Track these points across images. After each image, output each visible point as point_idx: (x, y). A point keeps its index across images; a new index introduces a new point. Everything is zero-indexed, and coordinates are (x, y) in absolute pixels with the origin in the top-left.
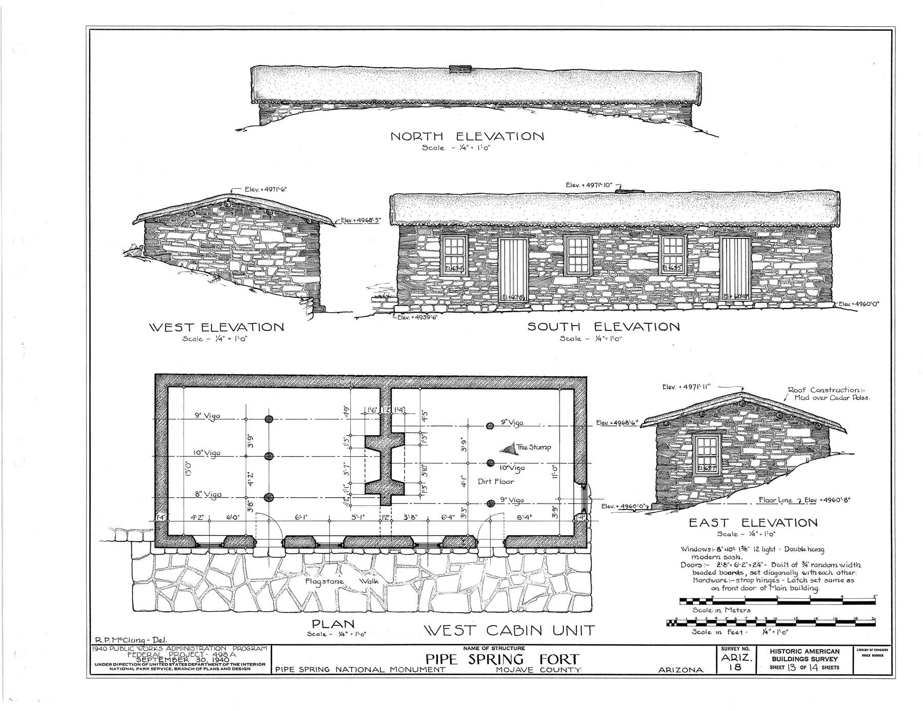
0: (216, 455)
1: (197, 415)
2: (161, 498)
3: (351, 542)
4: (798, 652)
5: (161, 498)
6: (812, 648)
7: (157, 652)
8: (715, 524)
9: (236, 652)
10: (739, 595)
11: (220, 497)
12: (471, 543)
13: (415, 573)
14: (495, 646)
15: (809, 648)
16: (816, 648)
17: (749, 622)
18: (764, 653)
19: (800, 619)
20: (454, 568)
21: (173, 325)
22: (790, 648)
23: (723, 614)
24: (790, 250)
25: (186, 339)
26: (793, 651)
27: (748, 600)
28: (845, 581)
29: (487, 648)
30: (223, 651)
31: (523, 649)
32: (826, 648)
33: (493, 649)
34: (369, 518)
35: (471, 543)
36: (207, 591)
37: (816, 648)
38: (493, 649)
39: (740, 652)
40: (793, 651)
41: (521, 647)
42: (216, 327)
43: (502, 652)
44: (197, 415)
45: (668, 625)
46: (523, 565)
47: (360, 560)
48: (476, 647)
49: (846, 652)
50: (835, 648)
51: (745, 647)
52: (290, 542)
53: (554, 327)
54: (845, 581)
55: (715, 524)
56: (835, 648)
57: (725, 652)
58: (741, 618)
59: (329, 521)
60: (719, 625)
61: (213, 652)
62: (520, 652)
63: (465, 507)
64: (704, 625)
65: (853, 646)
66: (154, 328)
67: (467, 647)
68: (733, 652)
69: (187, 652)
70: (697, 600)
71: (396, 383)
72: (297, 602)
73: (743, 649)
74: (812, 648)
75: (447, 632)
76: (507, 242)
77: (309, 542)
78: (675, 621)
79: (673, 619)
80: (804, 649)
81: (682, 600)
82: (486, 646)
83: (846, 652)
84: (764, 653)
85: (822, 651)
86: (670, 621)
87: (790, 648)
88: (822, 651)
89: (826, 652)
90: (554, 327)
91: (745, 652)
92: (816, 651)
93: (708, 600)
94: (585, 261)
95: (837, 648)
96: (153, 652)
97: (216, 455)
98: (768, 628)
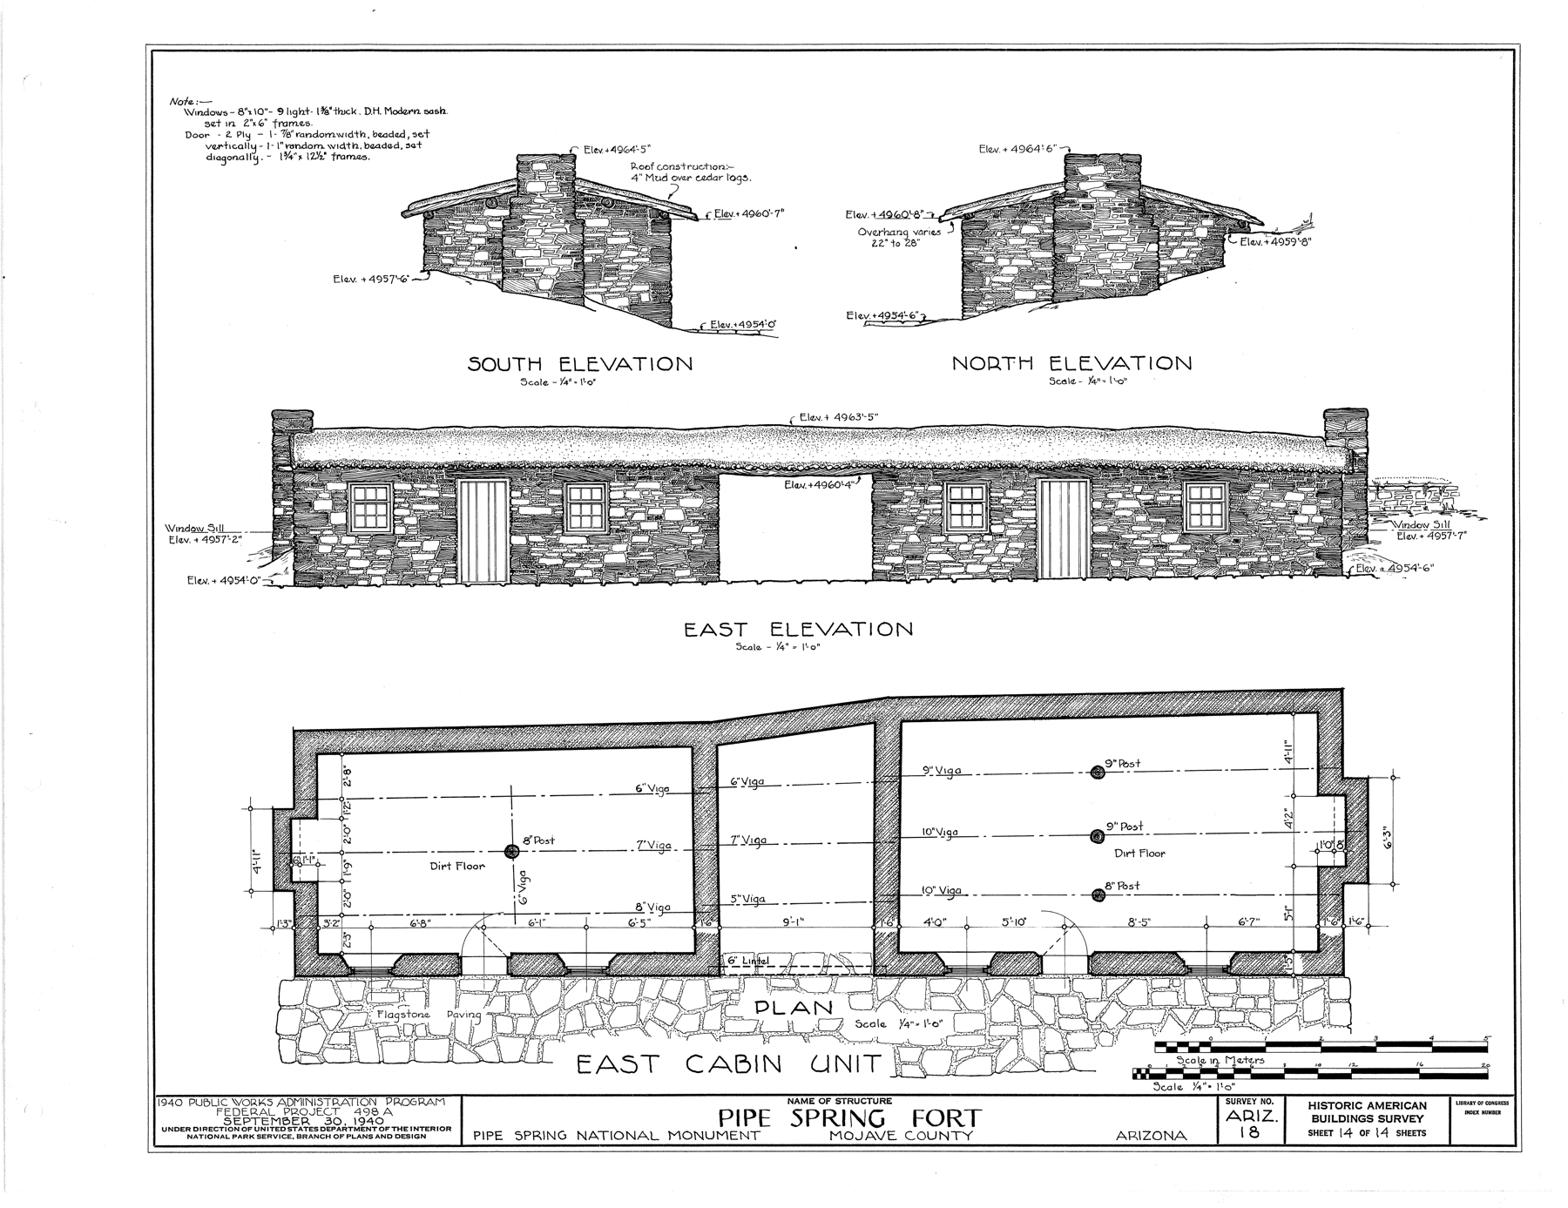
0: (952, 835)
1: (926, 769)
2: (888, 899)
3: (621, 964)
4: (1356, 1106)
5: (888, 899)
6: (1380, 1100)
9: (391, 1106)
10: (1257, 1039)
11: (960, 894)
12: (453, 966)
13: (950, 1003)
15: (1374, 1100)
16: (1386, 1099)
17: (1238, 1071)
18: (1298, 1108)
20: (715, 999)
22: (1343, 1100)
23: (1225, 1063)
24: (951, 539)
25: (740, 647)
26: (1347, 1105)
27: (1270, 1044)
29: (827, 1101)
30: (371, 1106)
32: (1404, 1099)
33: (838, 1102)
35: (1032, 965)
37: (1386, 1099)
38: (838, 1102)
39: (1257, 1106)
40: (1347, 1105)
41: (886, 1098)
43: (848, 1107)
44: (926, 769)
45: (1135, 1077)
46: (306, 995)
47: (627, 989)
49: (1438, 1107)
50: (1418, 1100)
52: (1106, 964)
56: (1418, 1100)
57: (1231, 1107)
60: (1221, 1077)
61: (355, 1107)
63: (1365, 923)
65: (1450, 1096)
67: (792, 1098)
68: (1246, 1107)
69: (311, 1109)
70: (1185, 1044)
72: (470, 1039)
73: (1263, 1102)
74: (1380, 1100)
76: (472, 486)
77: (1173, 967)
80: (1366, 1101)
81: (1158, 1044)
83: (1438, 1107)
84: (1298, 1108)
85: (1396, 1105)
86: (1139, 1070)
88: (1396, 1105)
89: (1404, 1106)
92: (1387, 1106)
95: (1423, 1100)
96: (260, 1109)
97: (952, 835)
98: (1201, 1082)
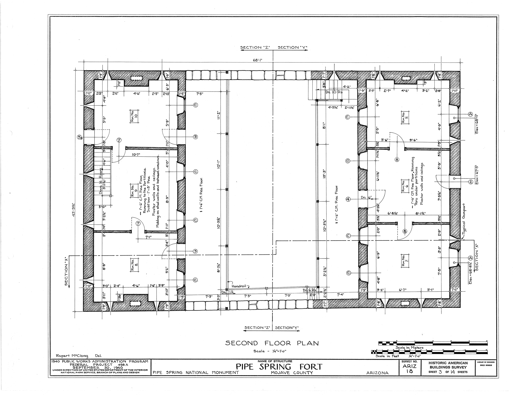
4: (444, 363)
6: (452, 361)
7: (85, 363)
14: (275, 360)
15: (450, 361)
19: (445, 350)
28: (71, 356)
29: (271, 361)
31: (291, 362)
33: (274, 361)
34: (439, 238)
38: (274, 361)
39: (412, 363)
43: (279, 363)
45: (372, 353)
48: (265, 360)
49: (471, 363)
50: (465, 361)
51: (415, 361)
54: (71, 356)
56: (465, 361)
58: (413, 350)
59: (405, 215)
62: (289, 363)
64: (381, 353)
66: (145, 169)
67: (259, 360)
68: (408, 363)
71: (88, 299)
74: (452, 361)
78: (376, 351)
79: (375, 349)
80: (448, 361)
81: (380, 342)
82: (270, 360)
83: (471, 363)
85: (457, 363)
86: (373, 351)
88: (457, 363)
89: (460, 363)
91: (415, 363)
92: (455, 363)
93: (395, 342)
95: (466, 361)
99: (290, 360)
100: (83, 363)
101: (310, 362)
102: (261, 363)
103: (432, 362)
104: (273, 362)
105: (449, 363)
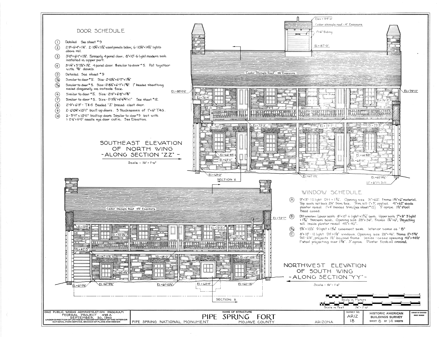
6: (390, 312)
8: (134, 144)
15: (388, 312)
16: (391, 312)
21: (316, 264)
26: (381, 313)
31: (251, 312)
36: (48, 311)
40: (381, 313)
42: (338, 265)
43: (239, 314)
45: (320, 305)
49: (406, 314)
50: (401, 312)
53: (110, 143)
55: (134, 144)
56: (401, 312)
58: (356, 302)
65: (410, 311)
74: (390, 312)
75: (314, 266)
80: (386, 312)
81: (327, 296)
83: (406, 314)
85: (394, 313)
87: (379, 312)
88: (394, 313)
90: (110, 143)
94: (268, 141)
95: (402, 312)
99: (250, 311)
100: (74, 314)
101: (266, 313)
102: (225, 313)
103: (373, 312)
104: (235, 313)
105: (387, 313)
